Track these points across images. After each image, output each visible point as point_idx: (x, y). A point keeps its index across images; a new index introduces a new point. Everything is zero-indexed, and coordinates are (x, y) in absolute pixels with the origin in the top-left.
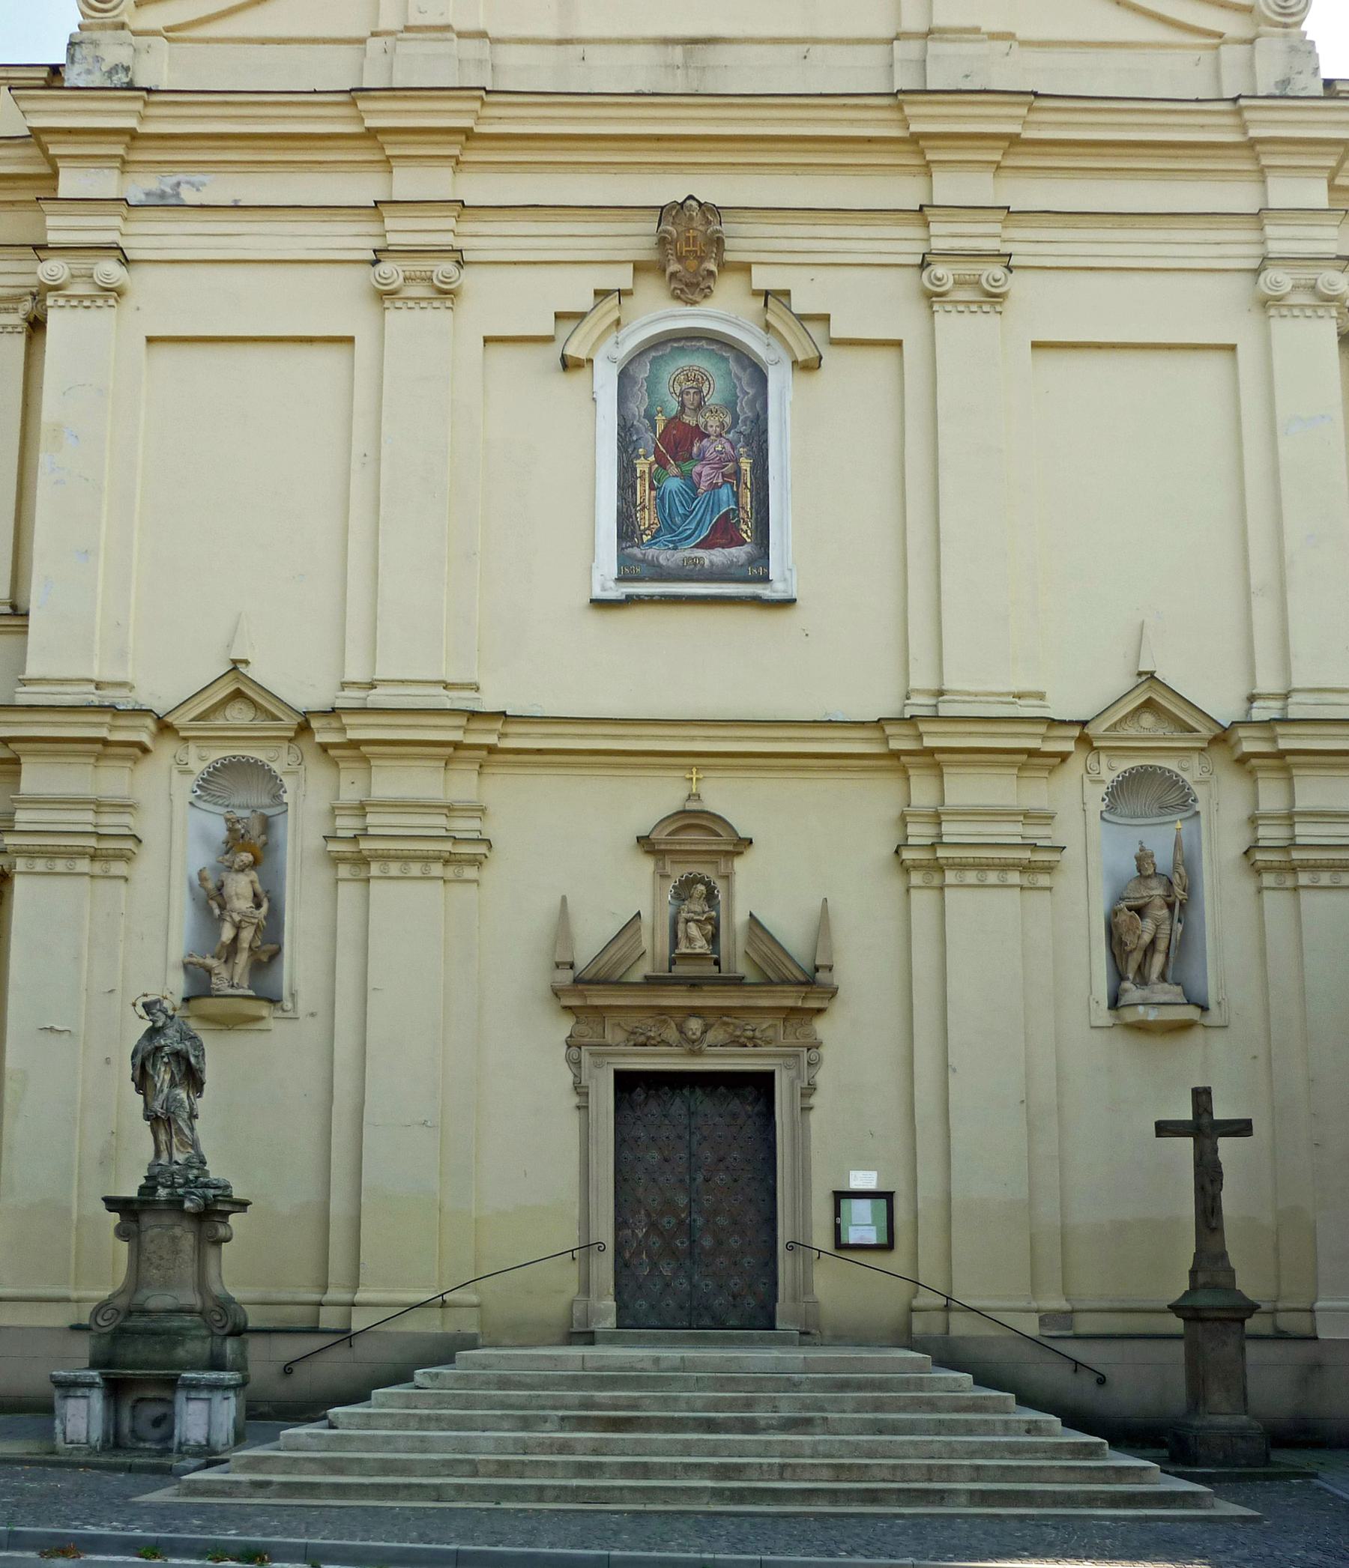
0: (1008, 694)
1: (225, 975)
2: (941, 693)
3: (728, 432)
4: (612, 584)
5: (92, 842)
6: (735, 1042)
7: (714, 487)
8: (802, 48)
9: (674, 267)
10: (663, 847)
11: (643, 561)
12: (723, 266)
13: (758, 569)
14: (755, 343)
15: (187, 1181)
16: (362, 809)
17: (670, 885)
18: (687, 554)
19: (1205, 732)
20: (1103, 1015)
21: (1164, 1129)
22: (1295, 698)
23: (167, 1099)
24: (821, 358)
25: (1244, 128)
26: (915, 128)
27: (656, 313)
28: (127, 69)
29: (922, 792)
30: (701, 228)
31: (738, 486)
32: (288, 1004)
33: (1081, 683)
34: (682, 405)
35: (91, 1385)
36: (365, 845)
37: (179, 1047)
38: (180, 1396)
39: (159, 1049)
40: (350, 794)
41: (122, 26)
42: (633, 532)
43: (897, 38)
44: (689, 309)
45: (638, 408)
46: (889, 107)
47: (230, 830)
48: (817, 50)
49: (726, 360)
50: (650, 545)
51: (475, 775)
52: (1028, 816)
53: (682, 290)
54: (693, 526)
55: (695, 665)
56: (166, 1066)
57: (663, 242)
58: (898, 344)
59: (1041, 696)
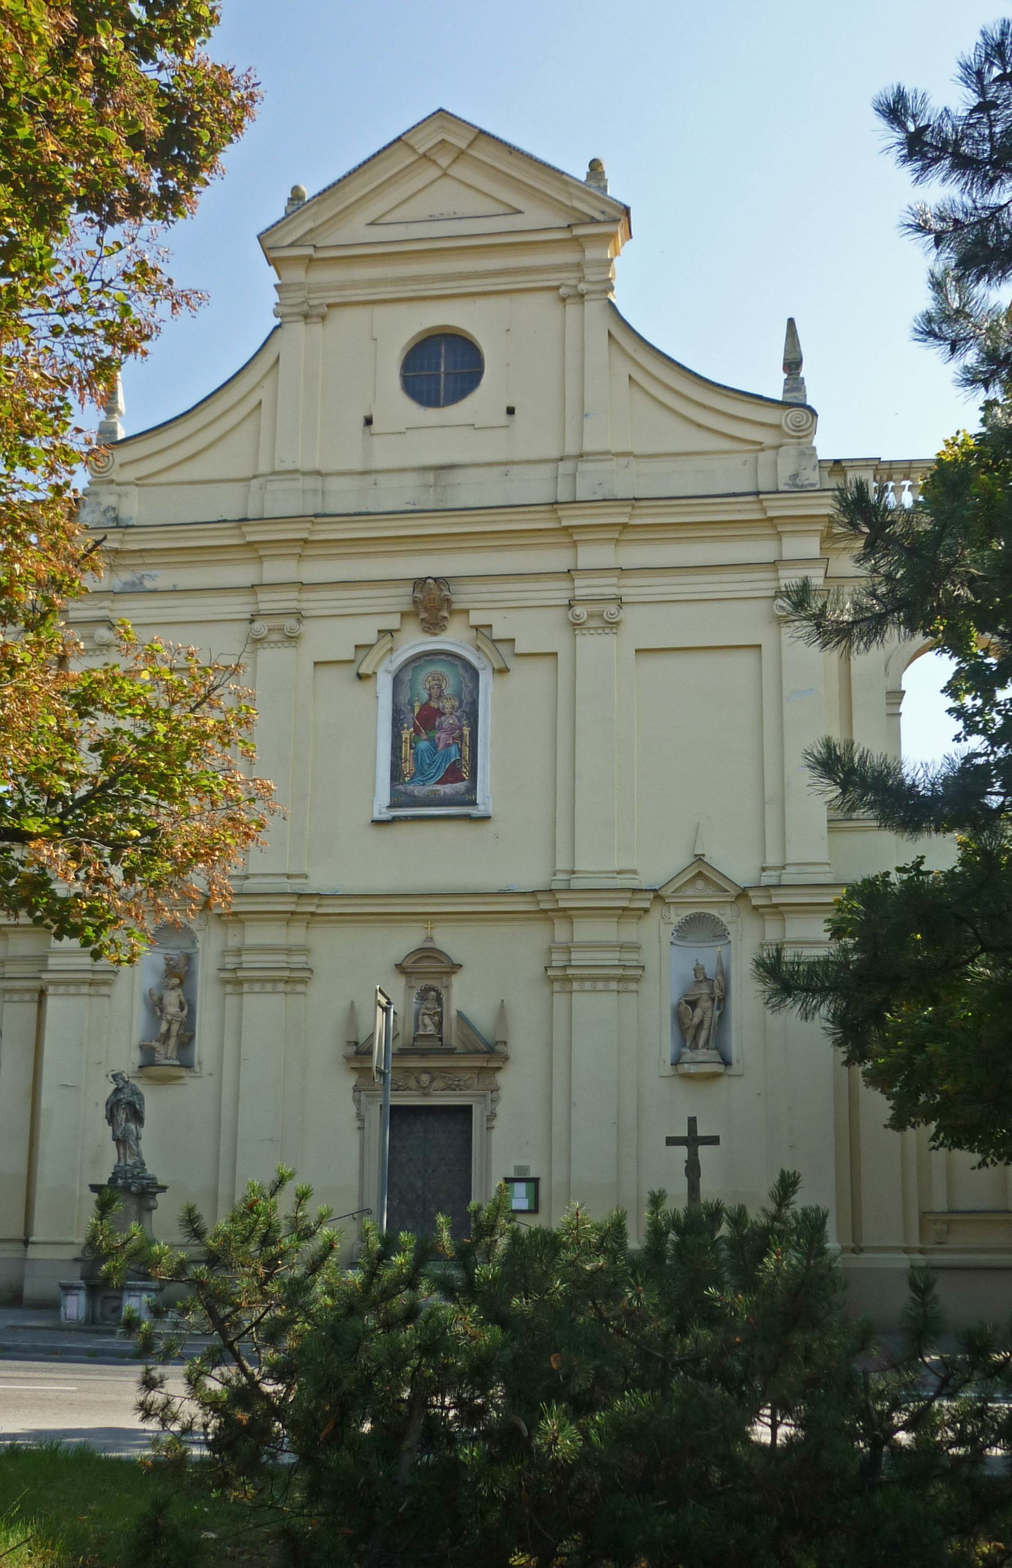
0: (613, 872)
1: (163, 1052)
2: (573, 872)
4: (385, 810)
5: (89, 976)
6: (449, 1088)
7: (448, 746)
8: (502, 469)
9: (423, 615)
10: (409, 970)
11: (405, 793)
12: (452, 612)
15: (133, 1176)
16: (239, 952)
17: (414, 993)
18: (431, 788)
19: (733, 892)
20: (668, 1069)
21: (671, 1141)
22: (790, 869)
23: (124, 1129)
25: (764, 510)
26: (565, 523)
27: (415, 641)
28: (114, 509)
29: (561, 933)
32: (197, 1069)
33: (659, 866)
34: (430, 695)
35: (79, 1288)
36: (240, 974)
37: (130, 1099)
38: (125, 1295)
39: (120, 1100)
40: (233, 942)
41: (112, 482)
43: (561, 459)
45: (404, 698)
46: (549, 511)
47: (167, 965)
48: (515, 468)
50: (409, 782)
51: (304, 929)
52: (622, 947)
55: (434, 857)
56: (124, 1109)
58: (556, 654)
59: (634, 872)
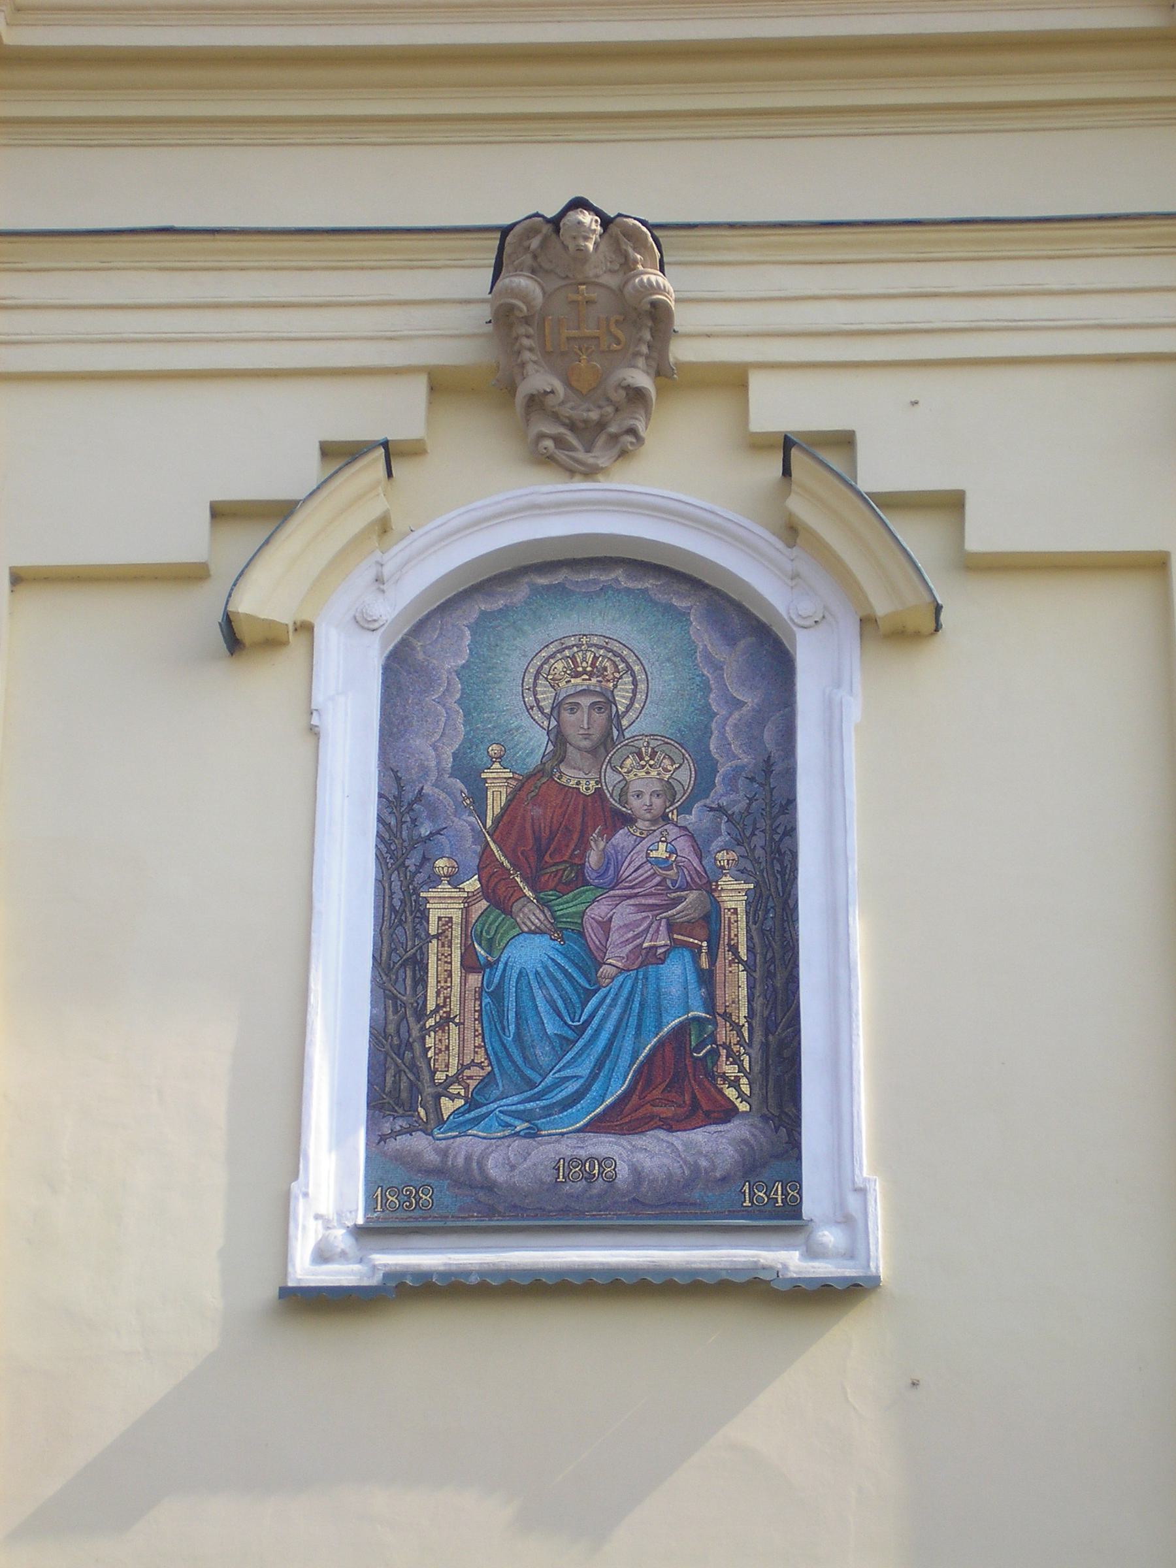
3: (685, 809)
11: (439, 1172)
13: (768, 1185)
14: (761, 577)
18: (567, 1148)
24: (938, 609)
27: (488, 503)
30: (606, 279)
31: (713, 960)
34: (559, 739)
42: (414, 1089)
44: (580, 488)
49: (681, 616)
50: (466, 1121)
53: (559, 441)
54: (584, 1069)
57: (506, 319)
